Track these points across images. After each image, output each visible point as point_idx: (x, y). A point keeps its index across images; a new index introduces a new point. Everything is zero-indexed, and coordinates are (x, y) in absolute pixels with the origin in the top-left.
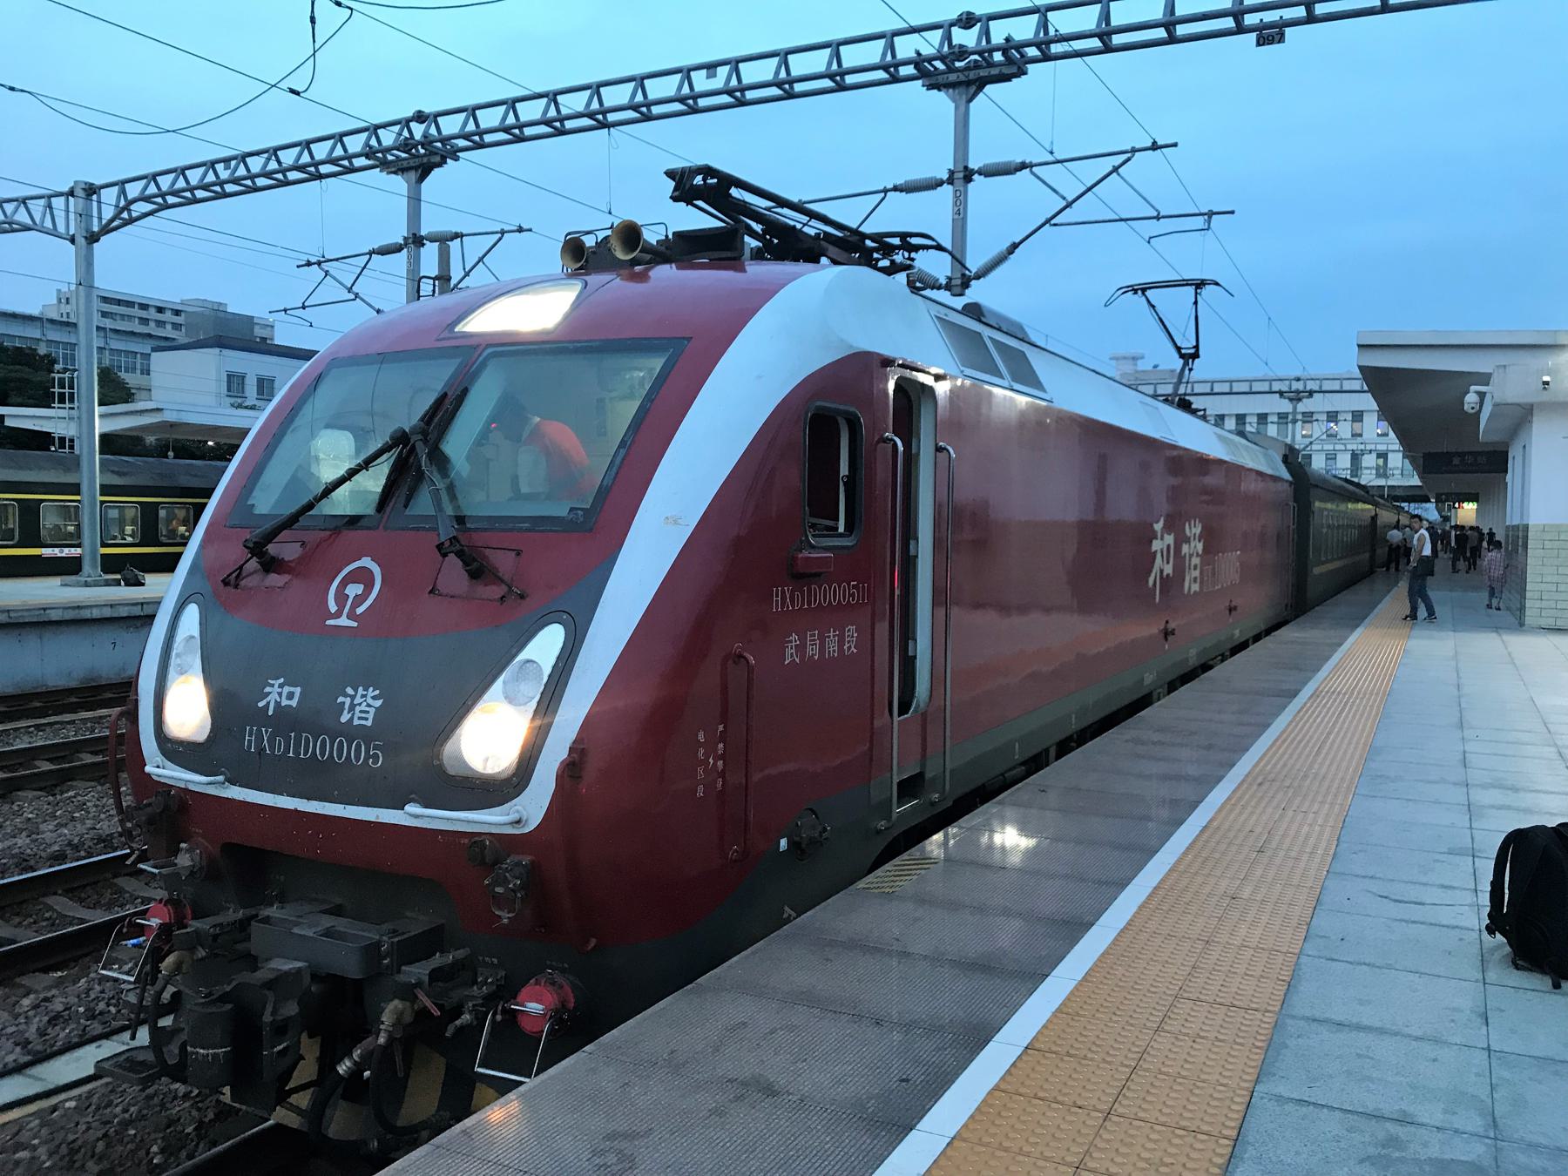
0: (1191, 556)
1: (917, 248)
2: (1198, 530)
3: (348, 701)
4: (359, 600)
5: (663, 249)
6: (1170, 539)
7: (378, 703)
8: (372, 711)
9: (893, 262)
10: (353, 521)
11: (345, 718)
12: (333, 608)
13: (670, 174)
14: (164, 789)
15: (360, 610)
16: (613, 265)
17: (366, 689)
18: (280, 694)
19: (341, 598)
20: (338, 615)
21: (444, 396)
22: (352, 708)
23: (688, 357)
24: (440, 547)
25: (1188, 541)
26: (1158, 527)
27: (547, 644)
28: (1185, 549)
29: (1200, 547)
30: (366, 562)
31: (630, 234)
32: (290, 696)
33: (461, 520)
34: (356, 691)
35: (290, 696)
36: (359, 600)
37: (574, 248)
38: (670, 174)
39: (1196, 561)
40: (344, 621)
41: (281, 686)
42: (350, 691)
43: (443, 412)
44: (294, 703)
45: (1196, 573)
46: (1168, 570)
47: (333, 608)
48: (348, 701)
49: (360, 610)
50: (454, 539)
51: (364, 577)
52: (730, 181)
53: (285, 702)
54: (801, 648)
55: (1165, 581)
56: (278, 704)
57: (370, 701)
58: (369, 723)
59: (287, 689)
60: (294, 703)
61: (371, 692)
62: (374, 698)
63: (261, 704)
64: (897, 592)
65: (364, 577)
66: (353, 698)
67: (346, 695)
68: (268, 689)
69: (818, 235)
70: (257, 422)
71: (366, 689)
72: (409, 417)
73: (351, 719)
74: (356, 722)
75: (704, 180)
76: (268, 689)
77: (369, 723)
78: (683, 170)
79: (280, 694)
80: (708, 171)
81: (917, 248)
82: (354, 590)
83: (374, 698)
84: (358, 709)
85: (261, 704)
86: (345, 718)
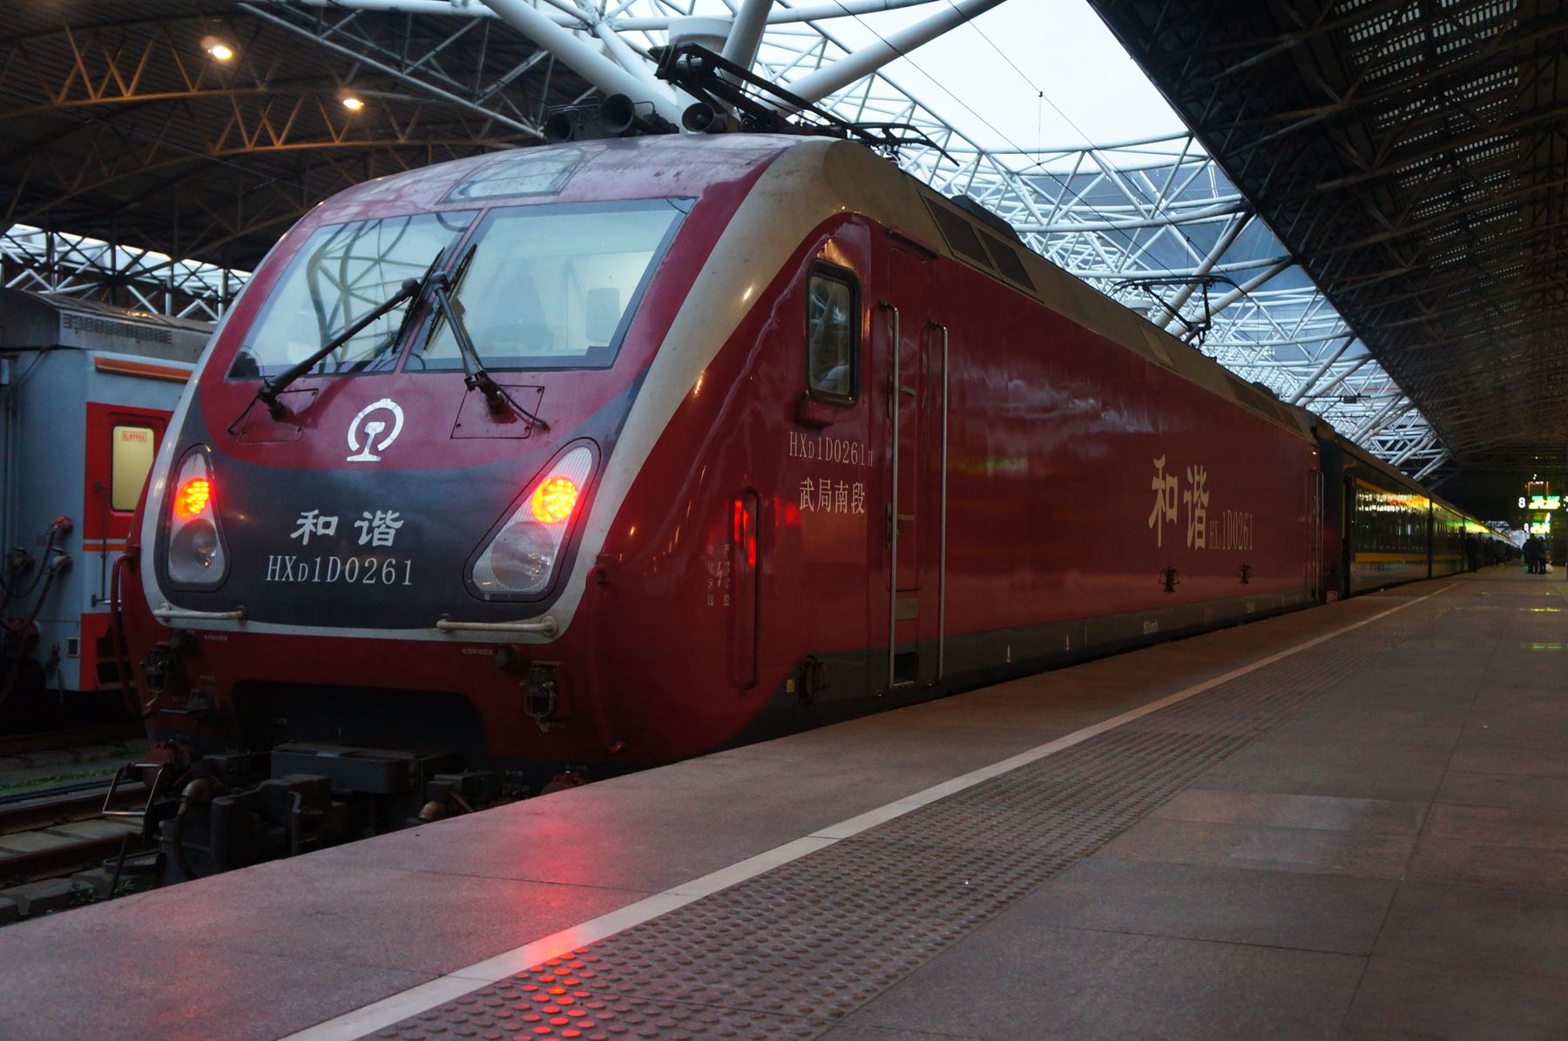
0: (1194, 506)
2: (1203, 479)
4: (381, 437)
6: (1173, 482)
7: (399, 524)
8: (392, 532)
10: (360, 367)
11: (363, 540)
12: (354, 445)
14: (166, 629)
15: (381, 447)
17: (385, 512)
18: (315, 525)
19: (362, 436)
20: (360, 451)
22: (371, 530)
24: (467, 381)
25: (1190, 487)
26: (1160, 464)
28: (1187, 496)
29: (1205, 499)
30: (386, 403)
32: (327, 525)
35: (327, 525)
36: (381, 437)
39: (1199, 513)
40: (367, 456)
41: (316, 517)
42: (367, 515)
44: (331, 532)
45: (1202, 527)
46: (1172, 514)
47: (354, 445)
48: (365, 525)
49: (381, 447)
53: (321, 531)
55: (1168, 526)
56: (313, 534)
57: (389, 522)
58: (389, 543)
59: (322, 519)
60: (331, 532)
61: (390, 515)
62: (394, 520)
63: (294, 535)
65: (386, 416)
66: (371, 521)
67: (364, 519)
68: (300, 522)
71: (385, 512)
74: (376, 543)
76: (300, 522)
77: (389, 543)
79: (315, 525)
82: (375, 428)
83: (394, 520)
84: (377, 531)
85: (294, 535)
86: (363, 540)
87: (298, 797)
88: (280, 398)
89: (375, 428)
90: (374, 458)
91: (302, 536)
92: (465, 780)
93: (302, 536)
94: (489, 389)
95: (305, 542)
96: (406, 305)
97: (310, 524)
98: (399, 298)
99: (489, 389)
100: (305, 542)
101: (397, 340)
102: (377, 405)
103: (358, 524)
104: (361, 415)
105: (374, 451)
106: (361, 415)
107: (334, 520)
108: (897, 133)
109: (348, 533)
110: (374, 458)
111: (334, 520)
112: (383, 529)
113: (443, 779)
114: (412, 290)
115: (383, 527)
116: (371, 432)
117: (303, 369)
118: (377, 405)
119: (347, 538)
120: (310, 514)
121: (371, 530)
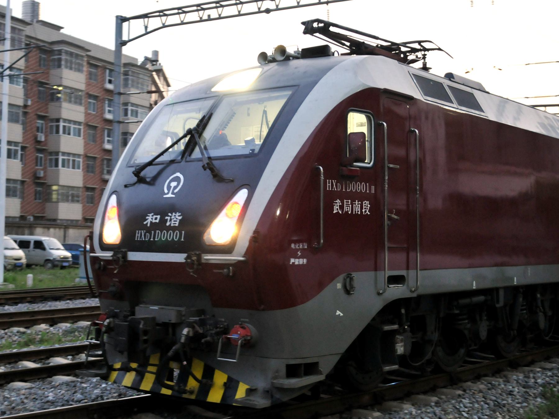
1: (428, 50)
3: (169, 218)
4: (175, 187)
5: (296, 54)
7: (180, 218)
8: (178, 221)
9: (417, 56)
10: (172, 162)
11: (168, 224)
12: (166, 191)
13: (303, 23)
16: (273, 60)
17: (176, 213)
19: (169, 187)
20: (168, 193)
21: (204, 117)
22: (171, 220)
23: (297, 94)
24: (203, 167)
27: (243, 194)
30: (178, 174)
31: (282, 50)
32: (156, 219)
33: (209, 158)
34: (172, 214)
35: (156, 219)
37: (263, 56)
38: (303, 23)
40: (170, 195)
41: (152, 216)
42: (170, 214)
43: (203, 123)
44: (157, 221)
47: (166, 191)
50: (208, 164)
51: (177, 179)
52: (328, 24)
53: (154, 221)
54: (342, 207)
56: (151, 222)
57: (177, 217)
58: (177, 225)
59: (155, 216)
60: (157, 221)
61: (178, 214)
62: (179, 216)
63: (145, 223)
64: (418, 172)
65: (177, 179)
66: (171, 217)
69: (377, 46)
70: (72, 126)
71: (176, 213)
72: (192, 124)
73: (170, 224)
74: (172, 225)
75: (318, 24)
76: (147, 218)
78: (308, 22)
79: (152, 219)
80: (319, 21)
81: (428, 50)
82: (174, 184)
83: (179, 216)
84: (173, 220)
85: (145, 223)
87: (142, 322)
88: (62, 230)
89: (174, 184)
90: (174, 196)
91: (147, 224)
92: (200, 319)
93: (147, 224)
94: (212, 170)
95: (149, 225)
96: (187, 139)
97: (151, 219)
98: (185, 136)
99: (212, 170)
100: (149, 225)
101: (183, 153)
102: (175, 175)
103: (166, 218)
104: (168, 181)
105: (173, 193)
106: (168, 181)
107: (159, 217)
108: (427, 45)
109: (163, 221)
110: (174, 196)
111: (159, 217)
112: (175, 220)
113: (192, 319)
114: (189, 132)
115: (174, 219)
116: (172, 187)
117: (150, 163)
118: (175, 175)
119: (161, 225)
120: (151, 215)
121: (171, 220)
